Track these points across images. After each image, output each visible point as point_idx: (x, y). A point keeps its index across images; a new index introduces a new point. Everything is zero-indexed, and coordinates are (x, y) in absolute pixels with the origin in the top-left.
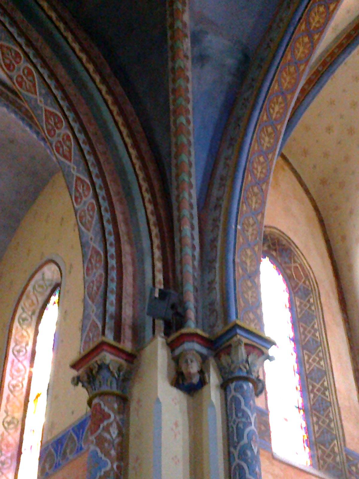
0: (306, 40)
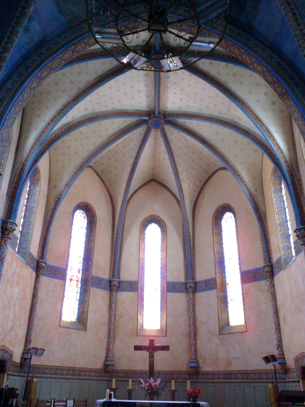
0: (71, 53)
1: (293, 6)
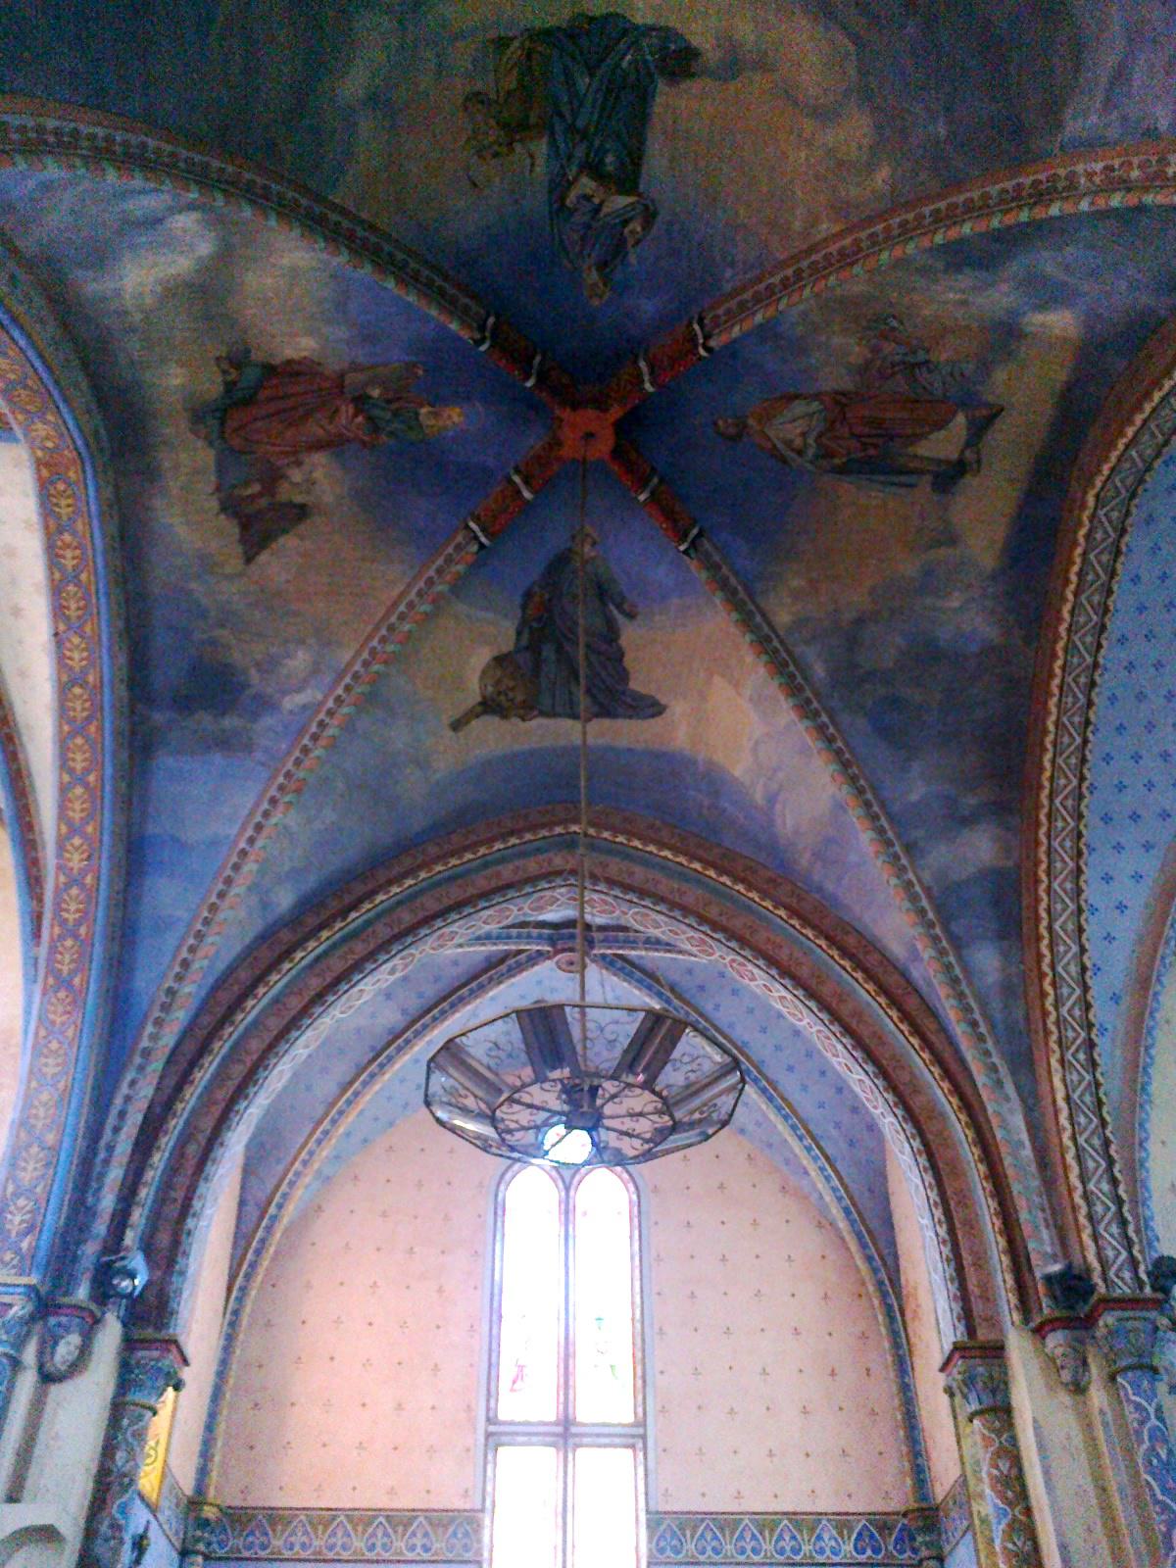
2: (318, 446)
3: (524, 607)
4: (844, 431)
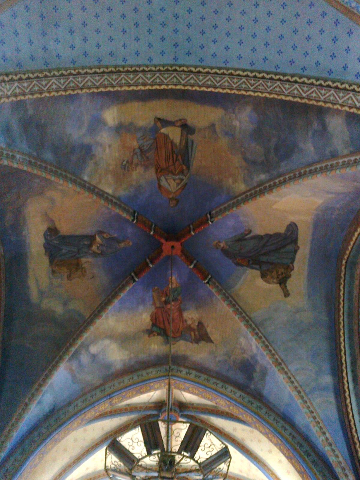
1: (296, 384)
2: (181, 314)
3: (242, 266)
4: (172, 168)
